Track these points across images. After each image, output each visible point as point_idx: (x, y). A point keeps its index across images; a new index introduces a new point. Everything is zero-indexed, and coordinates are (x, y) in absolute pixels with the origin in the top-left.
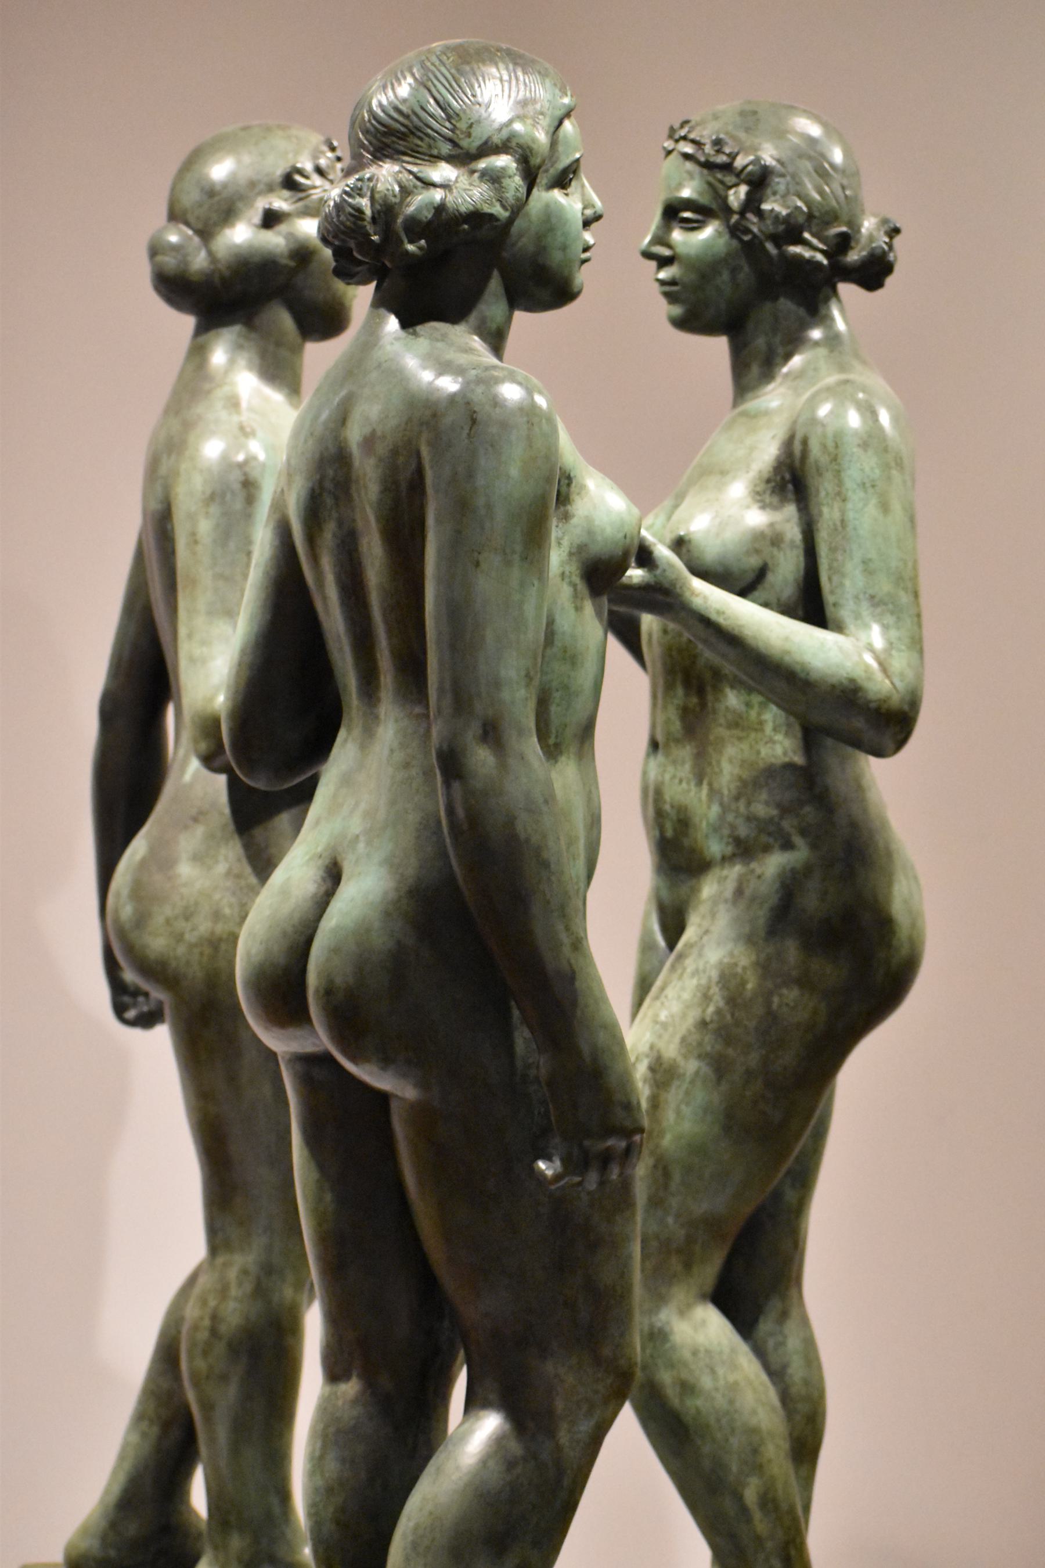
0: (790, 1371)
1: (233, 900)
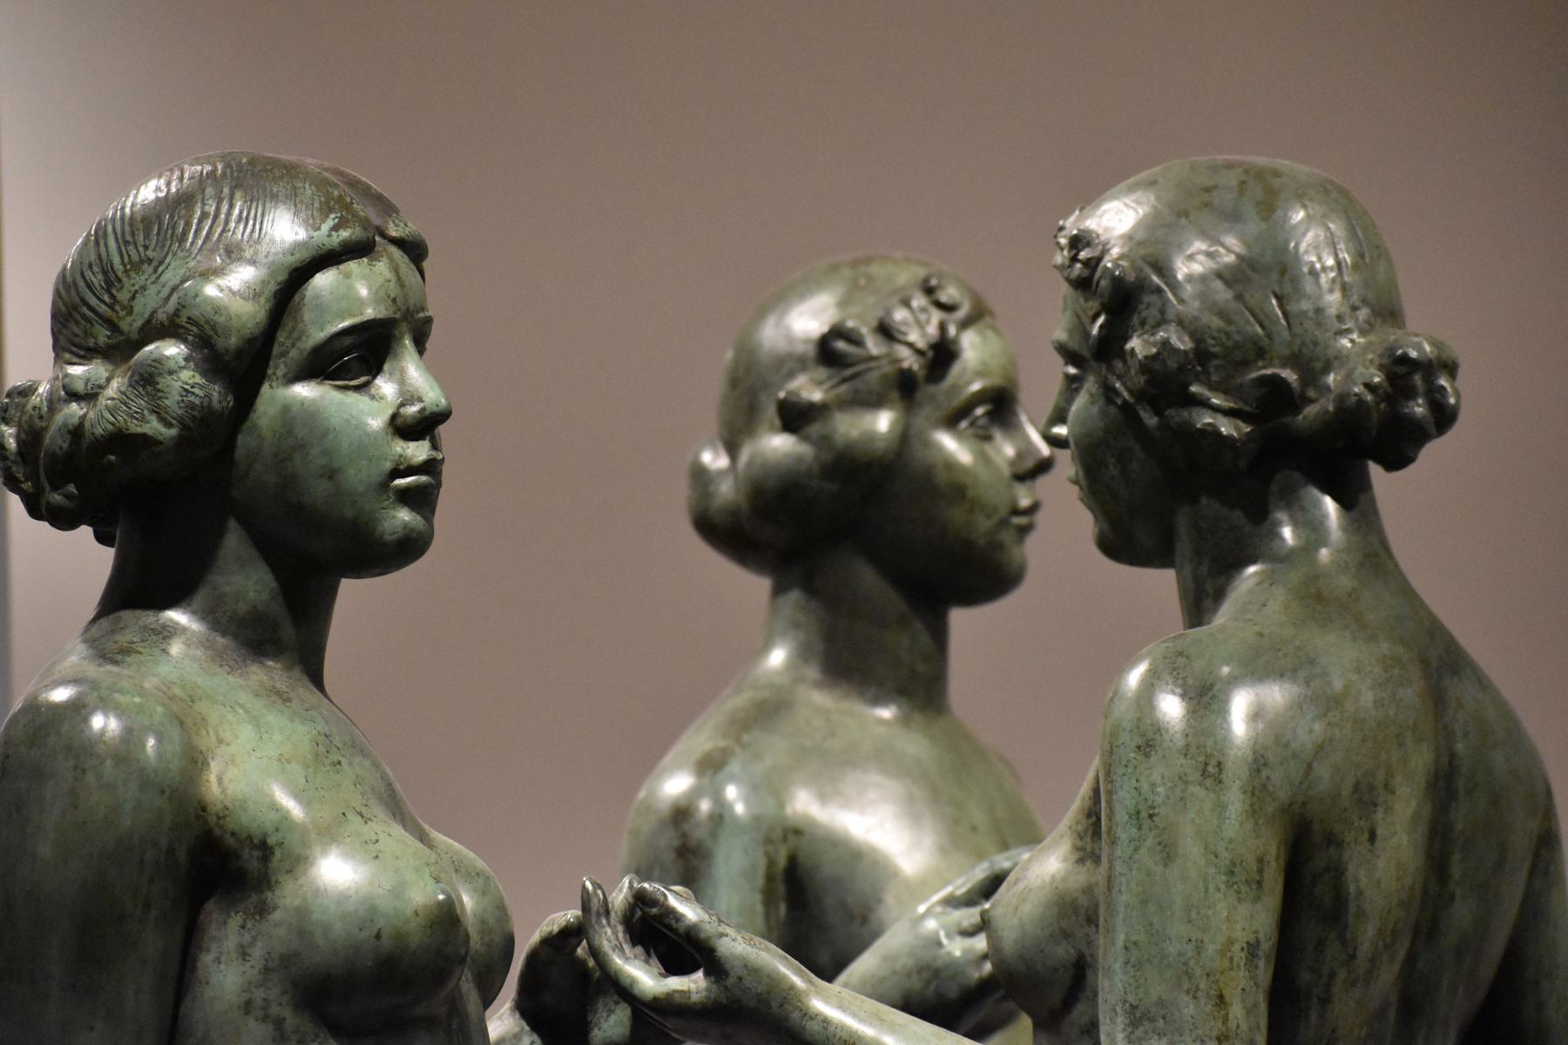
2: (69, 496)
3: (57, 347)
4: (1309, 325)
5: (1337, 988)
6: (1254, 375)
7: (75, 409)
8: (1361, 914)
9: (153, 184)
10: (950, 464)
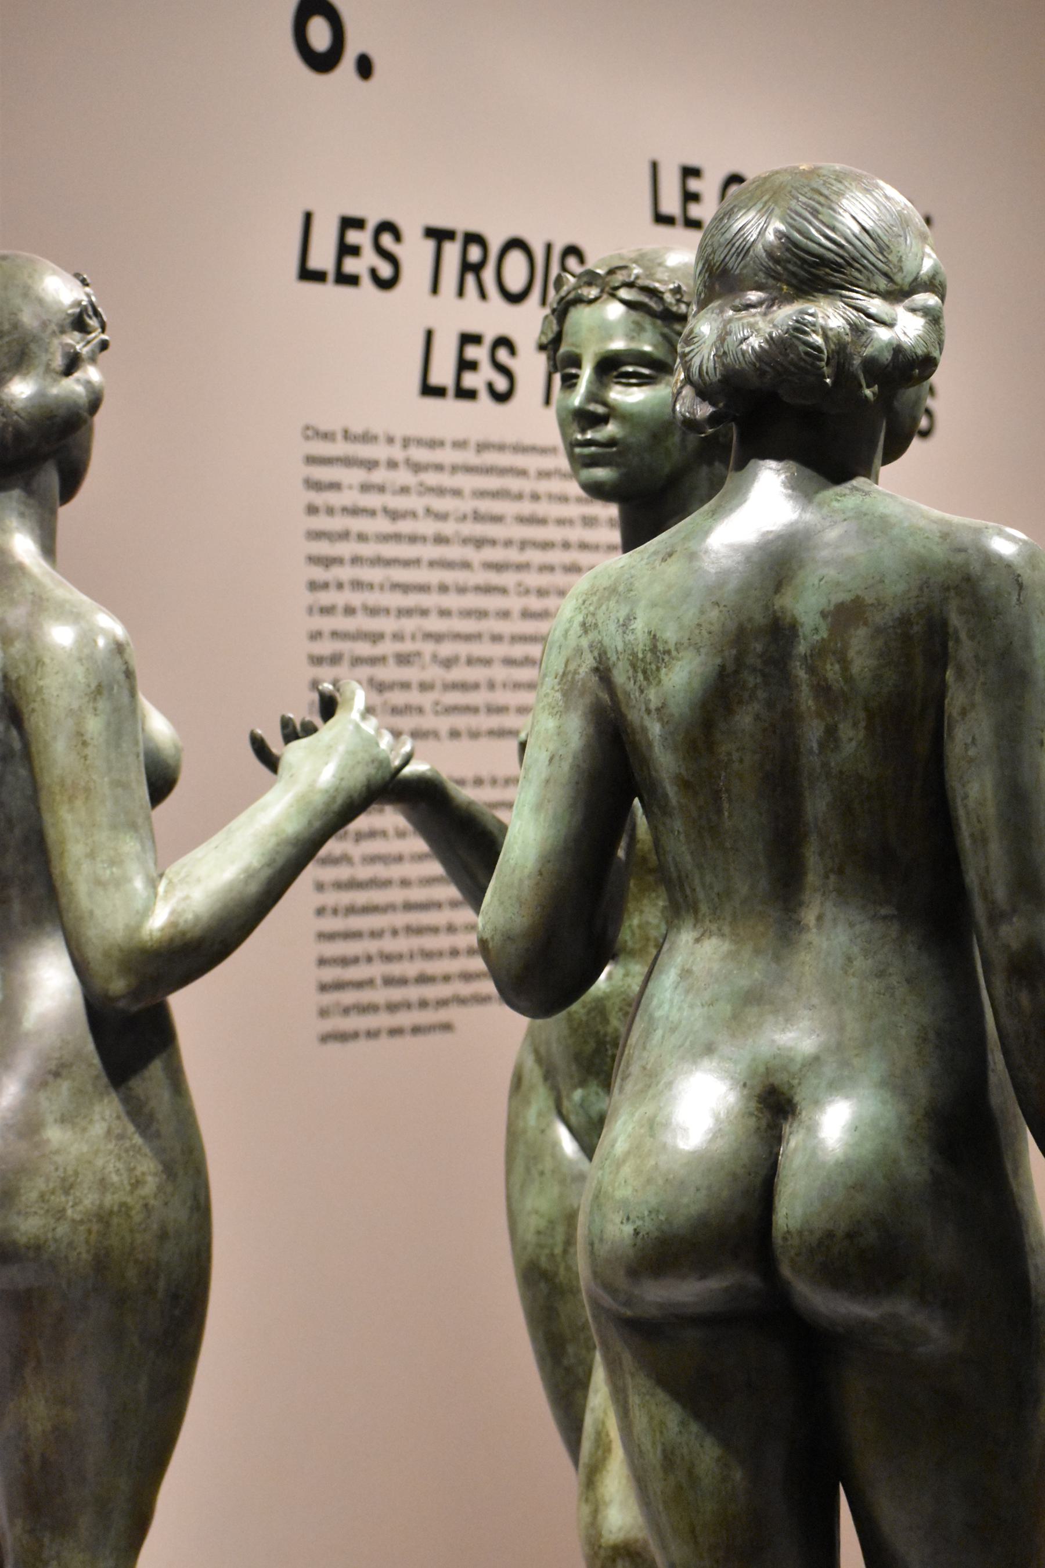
1: (120, 1165)
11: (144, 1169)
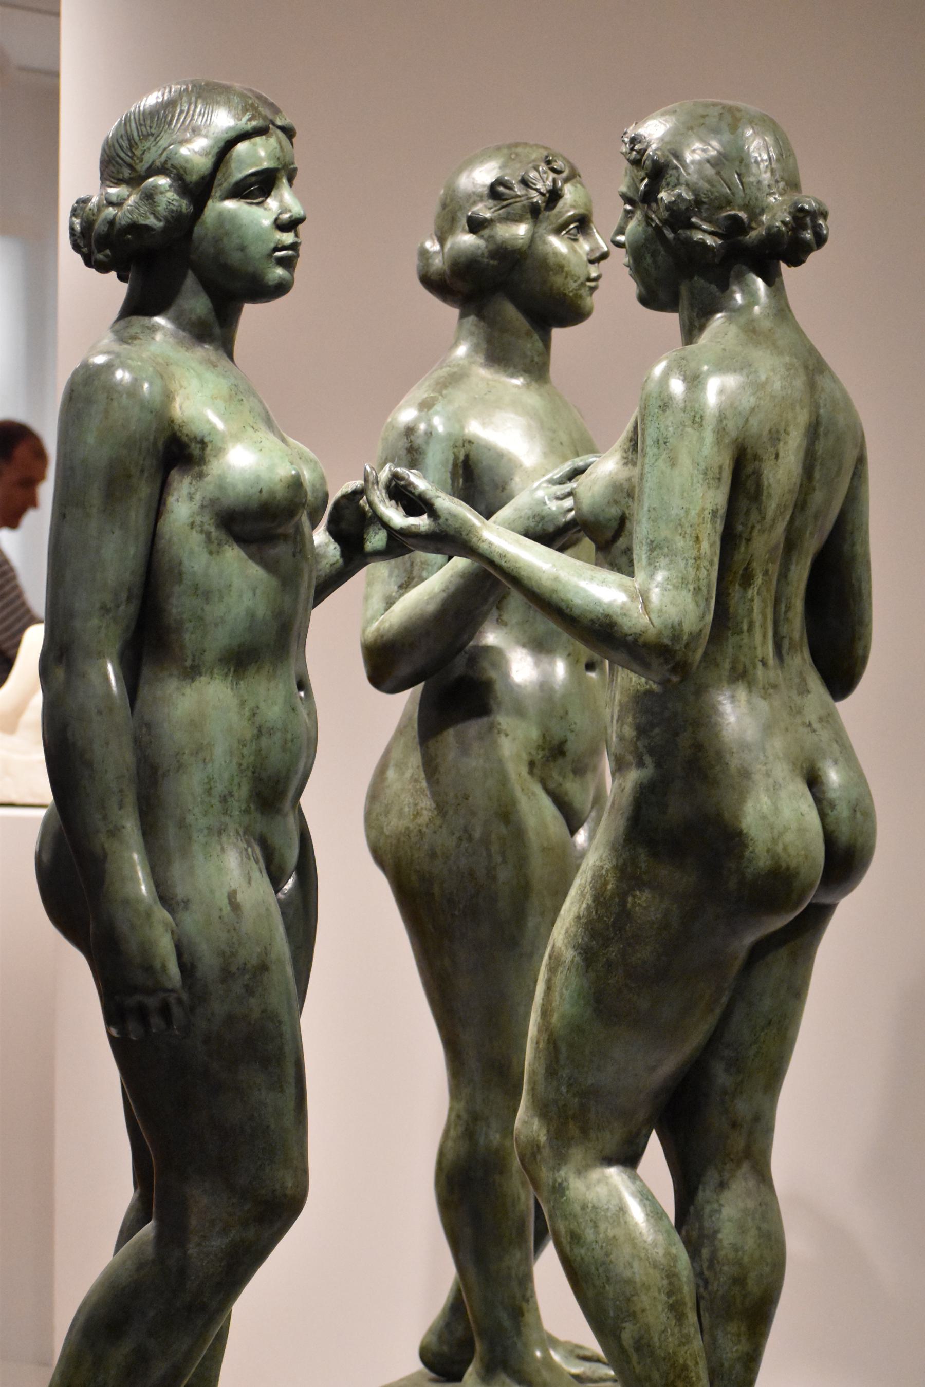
0: (720, 1236)
2: (107, 256)
3: (103, 178)
4: (754, 189)
5: (755, 533)
6: (724, 214)
7: (111, 211)
8: (769, 496)
9: (155, 94)
10: (556, 254)
11: (423, 805)
